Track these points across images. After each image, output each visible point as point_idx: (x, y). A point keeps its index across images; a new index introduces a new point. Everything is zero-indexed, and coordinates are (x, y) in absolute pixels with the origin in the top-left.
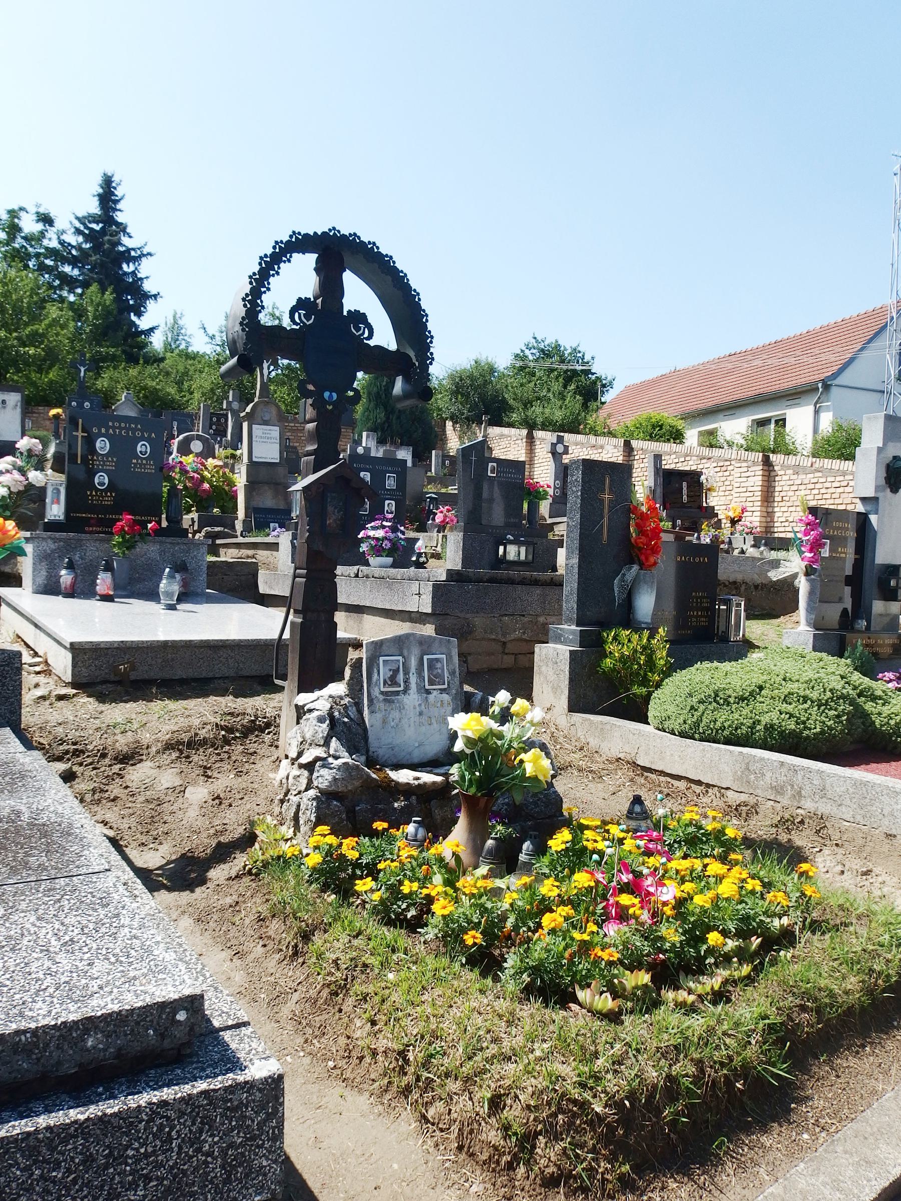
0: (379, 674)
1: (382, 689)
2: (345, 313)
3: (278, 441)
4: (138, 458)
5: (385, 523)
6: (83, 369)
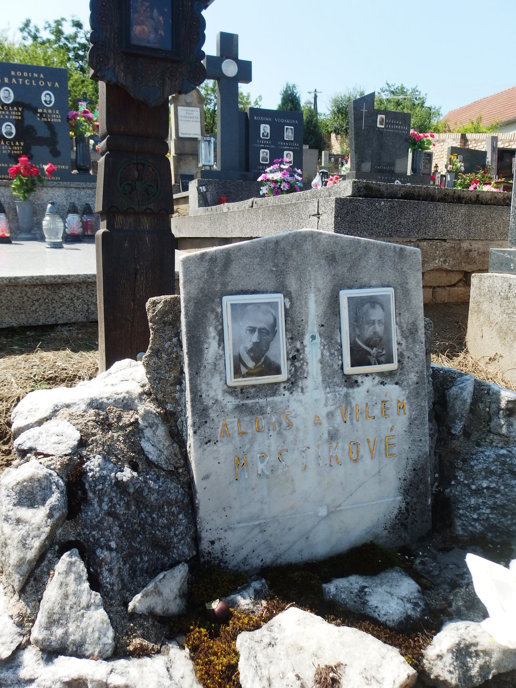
0: (221, 341)
1: (232, 381)
3: (199, 120)
4: (43, 107)
5: (282, 166)
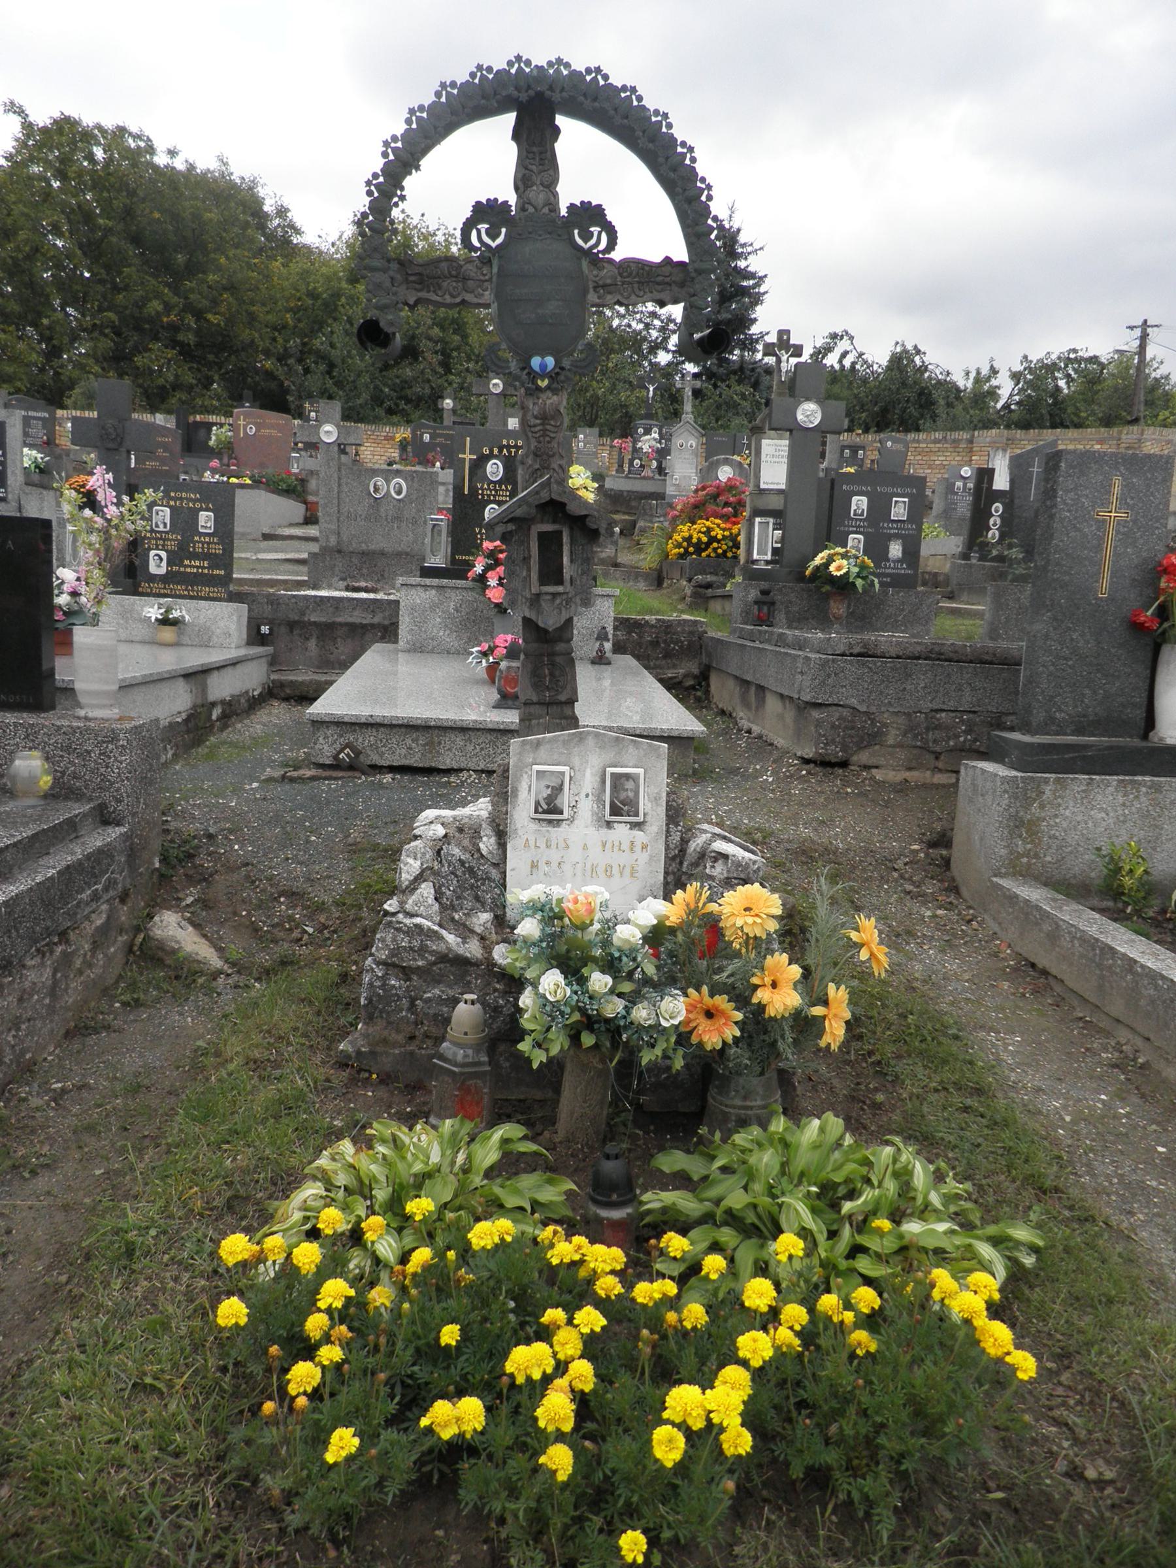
2: (563, 212)
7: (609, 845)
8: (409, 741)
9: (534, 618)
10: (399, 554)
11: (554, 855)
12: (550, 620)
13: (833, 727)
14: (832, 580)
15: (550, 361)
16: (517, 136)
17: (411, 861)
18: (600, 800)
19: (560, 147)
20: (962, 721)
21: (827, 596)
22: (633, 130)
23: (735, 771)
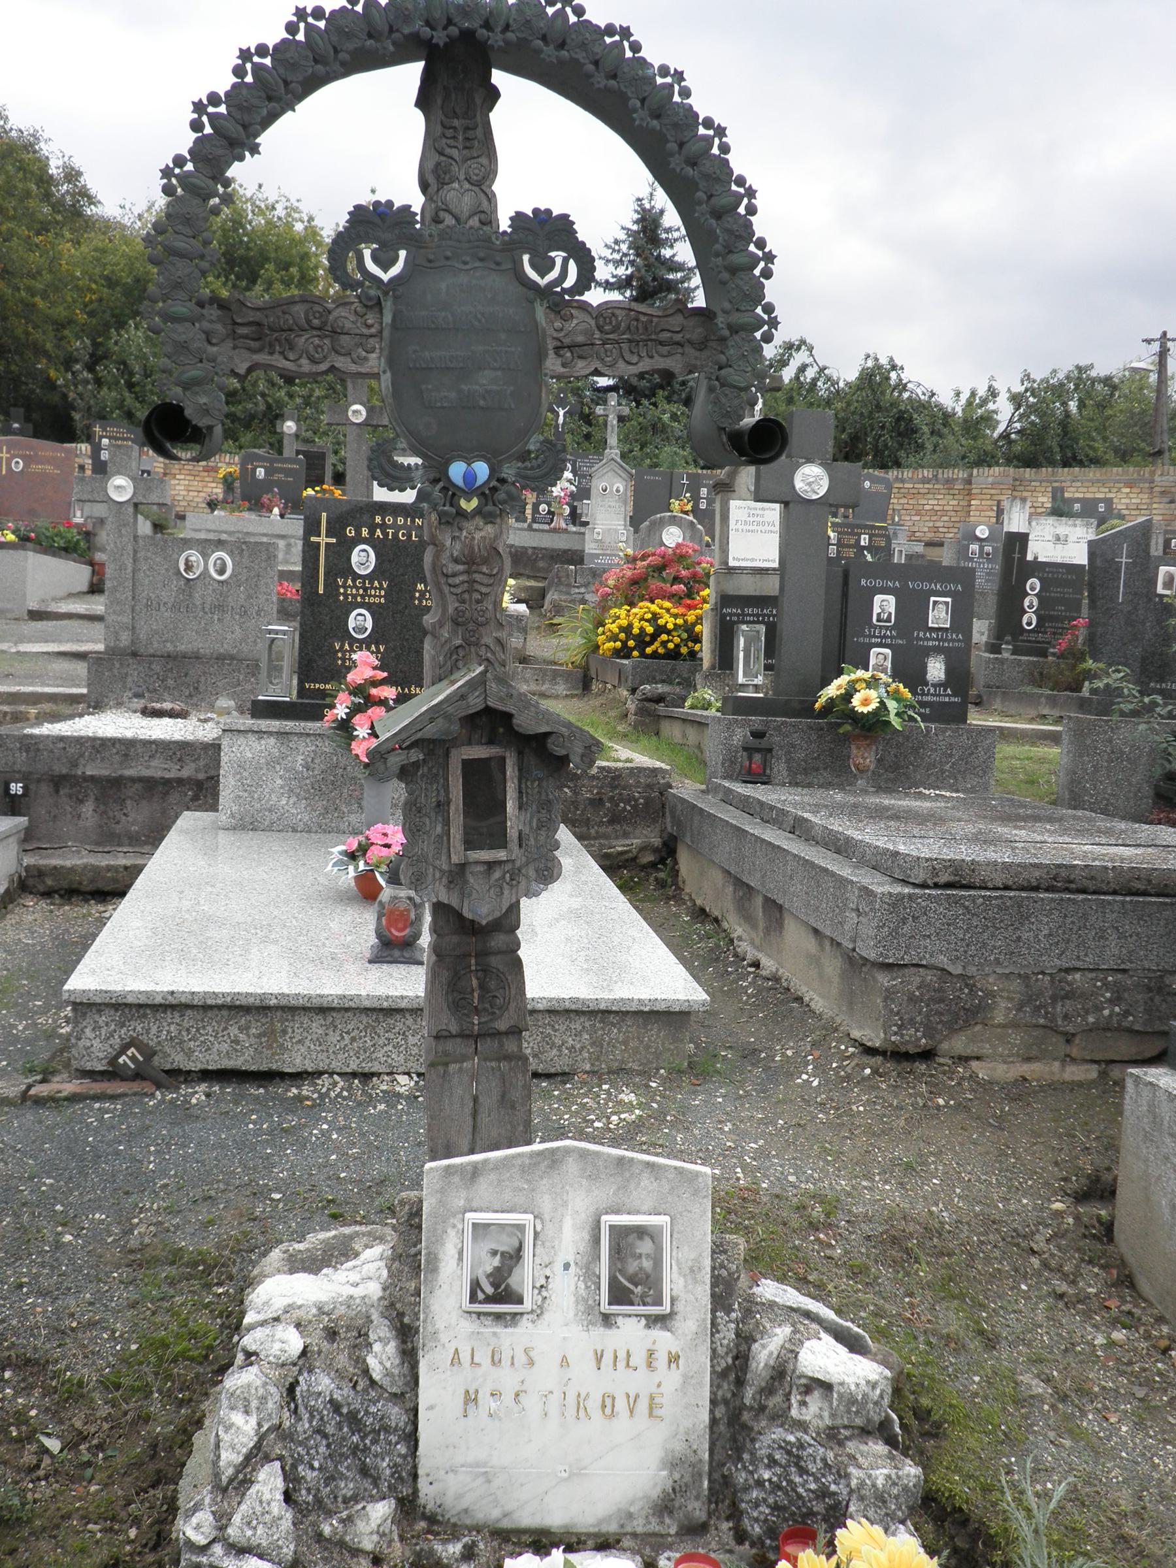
2: (504, 225)
3: (777, 528)
6: (561, 413)
7: (608, 1359)
8: (234, 1031)
9: (455, 903)
10: (220, 658)
11: (507, 1379)
12: (481, 909)
13: (912, 999)
14: (854, 717)
15: (482, 469)
16: (423, 101)
17: (237, 1418)
18: (590, 1276)
19: (498, 117)
20: (1106, 984)
21: (847, 737)
22: (624, 98)
23: (749, 1054)
